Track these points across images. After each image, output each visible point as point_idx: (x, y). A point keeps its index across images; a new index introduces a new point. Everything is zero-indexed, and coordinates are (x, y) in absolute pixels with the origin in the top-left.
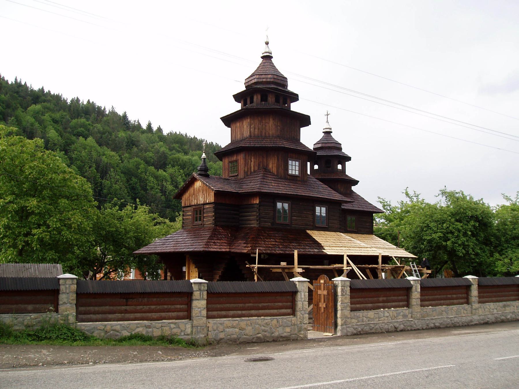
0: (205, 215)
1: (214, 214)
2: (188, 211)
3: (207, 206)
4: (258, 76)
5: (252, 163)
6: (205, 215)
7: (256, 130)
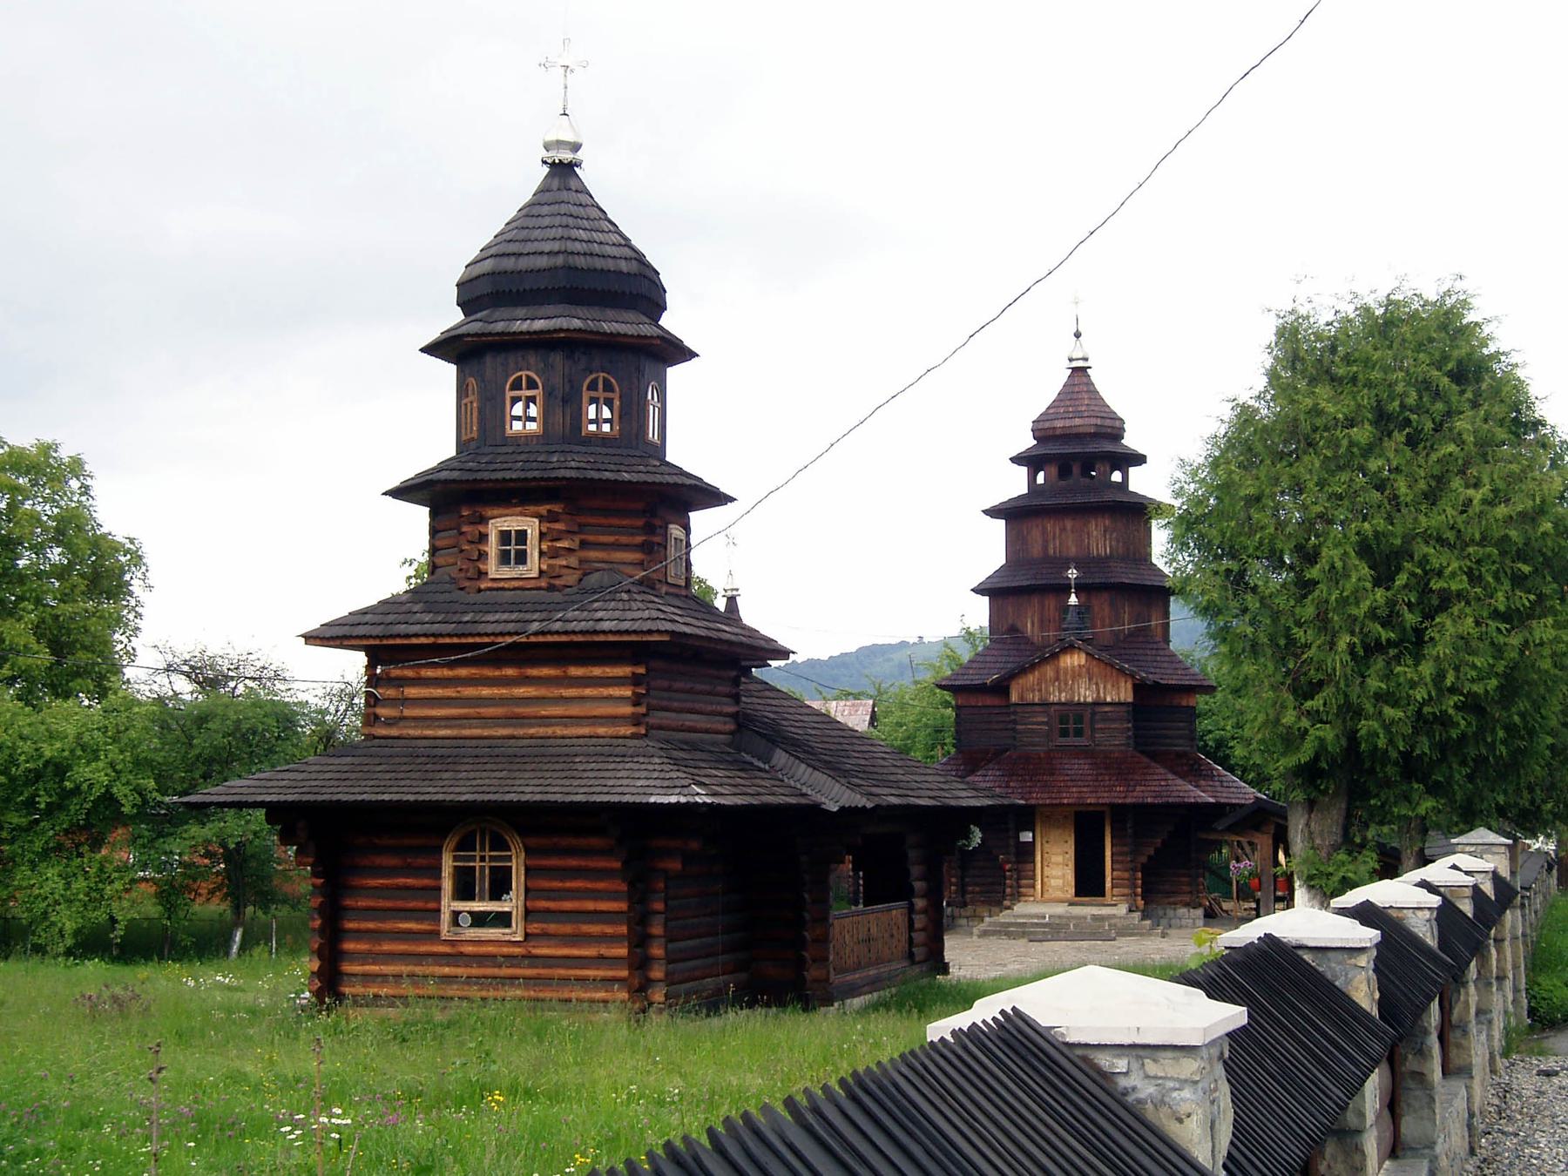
3: (1107, 709)
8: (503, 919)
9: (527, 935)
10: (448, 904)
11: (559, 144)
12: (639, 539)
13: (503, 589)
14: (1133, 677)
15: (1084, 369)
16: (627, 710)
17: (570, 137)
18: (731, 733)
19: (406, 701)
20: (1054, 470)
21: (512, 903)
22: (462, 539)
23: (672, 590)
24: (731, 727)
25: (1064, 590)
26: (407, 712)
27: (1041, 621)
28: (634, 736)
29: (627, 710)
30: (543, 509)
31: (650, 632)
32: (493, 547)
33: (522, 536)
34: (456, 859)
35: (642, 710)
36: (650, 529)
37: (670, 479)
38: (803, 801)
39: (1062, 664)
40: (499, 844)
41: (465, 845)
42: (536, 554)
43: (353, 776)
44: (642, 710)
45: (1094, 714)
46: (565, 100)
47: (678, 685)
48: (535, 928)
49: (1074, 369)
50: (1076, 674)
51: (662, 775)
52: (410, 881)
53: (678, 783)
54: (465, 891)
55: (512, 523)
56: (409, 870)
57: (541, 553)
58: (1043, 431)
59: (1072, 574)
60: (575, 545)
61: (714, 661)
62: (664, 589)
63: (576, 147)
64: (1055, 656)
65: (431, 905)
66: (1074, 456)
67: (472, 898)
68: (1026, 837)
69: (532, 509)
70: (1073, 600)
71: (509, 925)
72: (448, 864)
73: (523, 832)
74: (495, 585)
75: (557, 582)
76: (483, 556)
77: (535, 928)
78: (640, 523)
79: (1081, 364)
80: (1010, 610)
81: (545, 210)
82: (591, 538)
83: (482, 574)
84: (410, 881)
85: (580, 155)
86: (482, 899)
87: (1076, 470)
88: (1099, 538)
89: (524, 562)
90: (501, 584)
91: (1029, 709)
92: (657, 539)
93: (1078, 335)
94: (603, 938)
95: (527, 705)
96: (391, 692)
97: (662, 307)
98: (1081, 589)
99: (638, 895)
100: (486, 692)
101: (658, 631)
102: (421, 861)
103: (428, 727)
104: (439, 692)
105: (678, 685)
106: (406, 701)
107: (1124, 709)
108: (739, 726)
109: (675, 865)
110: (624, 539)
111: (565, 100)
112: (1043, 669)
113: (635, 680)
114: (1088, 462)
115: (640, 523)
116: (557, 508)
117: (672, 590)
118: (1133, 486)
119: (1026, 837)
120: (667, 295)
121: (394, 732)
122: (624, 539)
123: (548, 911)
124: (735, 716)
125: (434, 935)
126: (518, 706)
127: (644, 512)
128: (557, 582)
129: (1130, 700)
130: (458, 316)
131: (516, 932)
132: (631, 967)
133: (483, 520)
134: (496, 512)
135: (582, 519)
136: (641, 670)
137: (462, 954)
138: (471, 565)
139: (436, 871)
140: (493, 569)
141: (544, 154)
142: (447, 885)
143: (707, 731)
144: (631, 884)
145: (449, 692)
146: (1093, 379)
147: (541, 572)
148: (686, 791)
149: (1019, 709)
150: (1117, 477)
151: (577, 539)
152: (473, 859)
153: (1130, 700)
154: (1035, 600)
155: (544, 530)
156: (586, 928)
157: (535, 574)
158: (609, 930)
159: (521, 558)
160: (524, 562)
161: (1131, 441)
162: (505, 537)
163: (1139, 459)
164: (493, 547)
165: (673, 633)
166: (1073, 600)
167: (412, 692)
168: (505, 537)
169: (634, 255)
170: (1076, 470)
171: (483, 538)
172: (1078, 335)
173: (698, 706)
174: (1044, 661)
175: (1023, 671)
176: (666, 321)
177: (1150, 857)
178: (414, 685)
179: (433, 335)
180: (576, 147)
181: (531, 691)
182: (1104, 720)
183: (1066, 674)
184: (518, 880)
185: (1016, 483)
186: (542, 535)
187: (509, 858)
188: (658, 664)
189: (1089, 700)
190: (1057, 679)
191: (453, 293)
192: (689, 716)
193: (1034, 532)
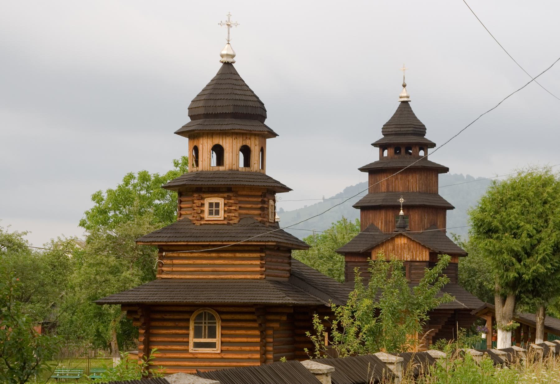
3: (417, 264)
8: (213, 345)
9: (222, 351)
10: (192, 340)
11: (228, 55)
12: (260, 206)
13: (210, 224)
14: (429, 249)
15: (406, 102)
16: (258, 269)
17: (231, 53)
18: (288, 277)
19: (173, 265)
20: (392, 151)
21: (217, 340)
22: (195, 205)
23: (271, 224)
24: (288, 275)
25: (397, 208)
26: (174, 269)
27: (386, 222)
28: (261, 279)
29: (258, 269)
30: (225, 195)
31: (268, 241)
32: (206, 208)
33: (217, 205)
34: (195, 323)
35: (264, 269)
36: (263, 202)
37: (273, 185)
38: (317, 303)
39: (396, 243)
40: (212, 317)
41: (199, 317)
42: (223, 212)
43: (159, 293)
44: (264, 269)
45: (411, 266)
46: (229, 37)
47: (273, 260)
48: (225, 348)
49: (403, 102)
50: (403, 248)
51: (274, 293)
52: (178, 331)
53: (281, 296)
54: (198, 334)
55: (214, 200)
56: (181, 328)
57: (225, 211)
58: (387, 130)
59: (402, 200)
60: (237, 208)
61: (280, 248)
62: (268, 224)
63: (233, 56)
64: (393, 239)
65: (185, 340)
66: (403, 144)
67: (201, 338)
69: (222, 195)
70: (401, 213)
71: (215, 347)
72: (192, 325)
73: (220, 313)
74: (207, 222)
75: (231, 222)
76: (202, 211)
77: (225, 348)
78: (260, 200)
79: (406, 99)
80: (371, 216)
81: (223, 82)
82: (242, 206)
83: (202, 218)
84: (178, 331)
85: (235, 59)
86: (205, 338)
87: (403, 151)
88: (414, 183)
89: (218, 214)
90: (210, 222)
92: (266, 206)
93: (404, 86)
94: (250, 352)
95: (220, 267)
96: (169, 262)
97: (264, 117)
98: (406, 207)
99: (263, 336)
100: (205, 262)
101: (272, 241)
102: (182, 324)
103: (182, 275)
104: (186, 262)
105: (273, 260)
106: (173, 265)
107: (425, 264)
108: (291, 275)
109: (276, 325)
110: (254, 206)
111: (229, 37)
112: (387, 245)
113: (261, 258)
114: (409, 146)
115: (260, 200)
116: (231, 194)
117: (271, 224)
118: (430, 158)
120: (267, 113)
121: (169, 276)
122: (254, 206)
123: (230, 342)
124: (289, 271)
125: (187, 351)
126: (216, 267)
127: (261, 196)
128: (231, 222)
129: (428, 259)
130: (189, 120)
131: (218, 349)
132: (261, 362)
133: (203, 199)
134: (207, 195)
135: (240, 199)
136: (263, 255)
137: (197, 358)
138: (198, 215)
139: (188, 328)
140: (206, 216)
141: (220, 58)
142: (192, 333)
143: (281, 277)
144: (261, 332)
145: (191, 262)
146: (411, 105)
147: (225, 218)
148: (284, 299)
150: (422, 153)
151: (238, 205)
152: (202, 323)
153: (428, 259)
154: (383, 213)
155: (226, 202)
156: (244, 348)
157: (222, 219)
158: (252, 348)
159: (217, 213)
160: (218, 214)
161: (429, 136)
162: (211, 205)
163: (433, 145)
164: (206, 208)
165: (277, 242)
166: (401, 213)
167: (175, 262)
168: (211, 205)
169: (256, 99)
170: (403, 151)
171: (203, 205)
172: (404, 86)
173: (279, 267)
174: (388, 241)
175: (378, 246)
176: (266, 122)
178: (177, 259)
179: (178, 127)
180: (233, 56)
181: (221, 262)
182: (416, 269)
183: (398, 247)
184: (218, 332)
185: (373, 156)
186: (225, 204)
187: (215, 323)
188: (268, 252)
189: (409, 259)
190: (394, 249)
191: (187, 111)
192: (277, 271)
193: (383, 180)
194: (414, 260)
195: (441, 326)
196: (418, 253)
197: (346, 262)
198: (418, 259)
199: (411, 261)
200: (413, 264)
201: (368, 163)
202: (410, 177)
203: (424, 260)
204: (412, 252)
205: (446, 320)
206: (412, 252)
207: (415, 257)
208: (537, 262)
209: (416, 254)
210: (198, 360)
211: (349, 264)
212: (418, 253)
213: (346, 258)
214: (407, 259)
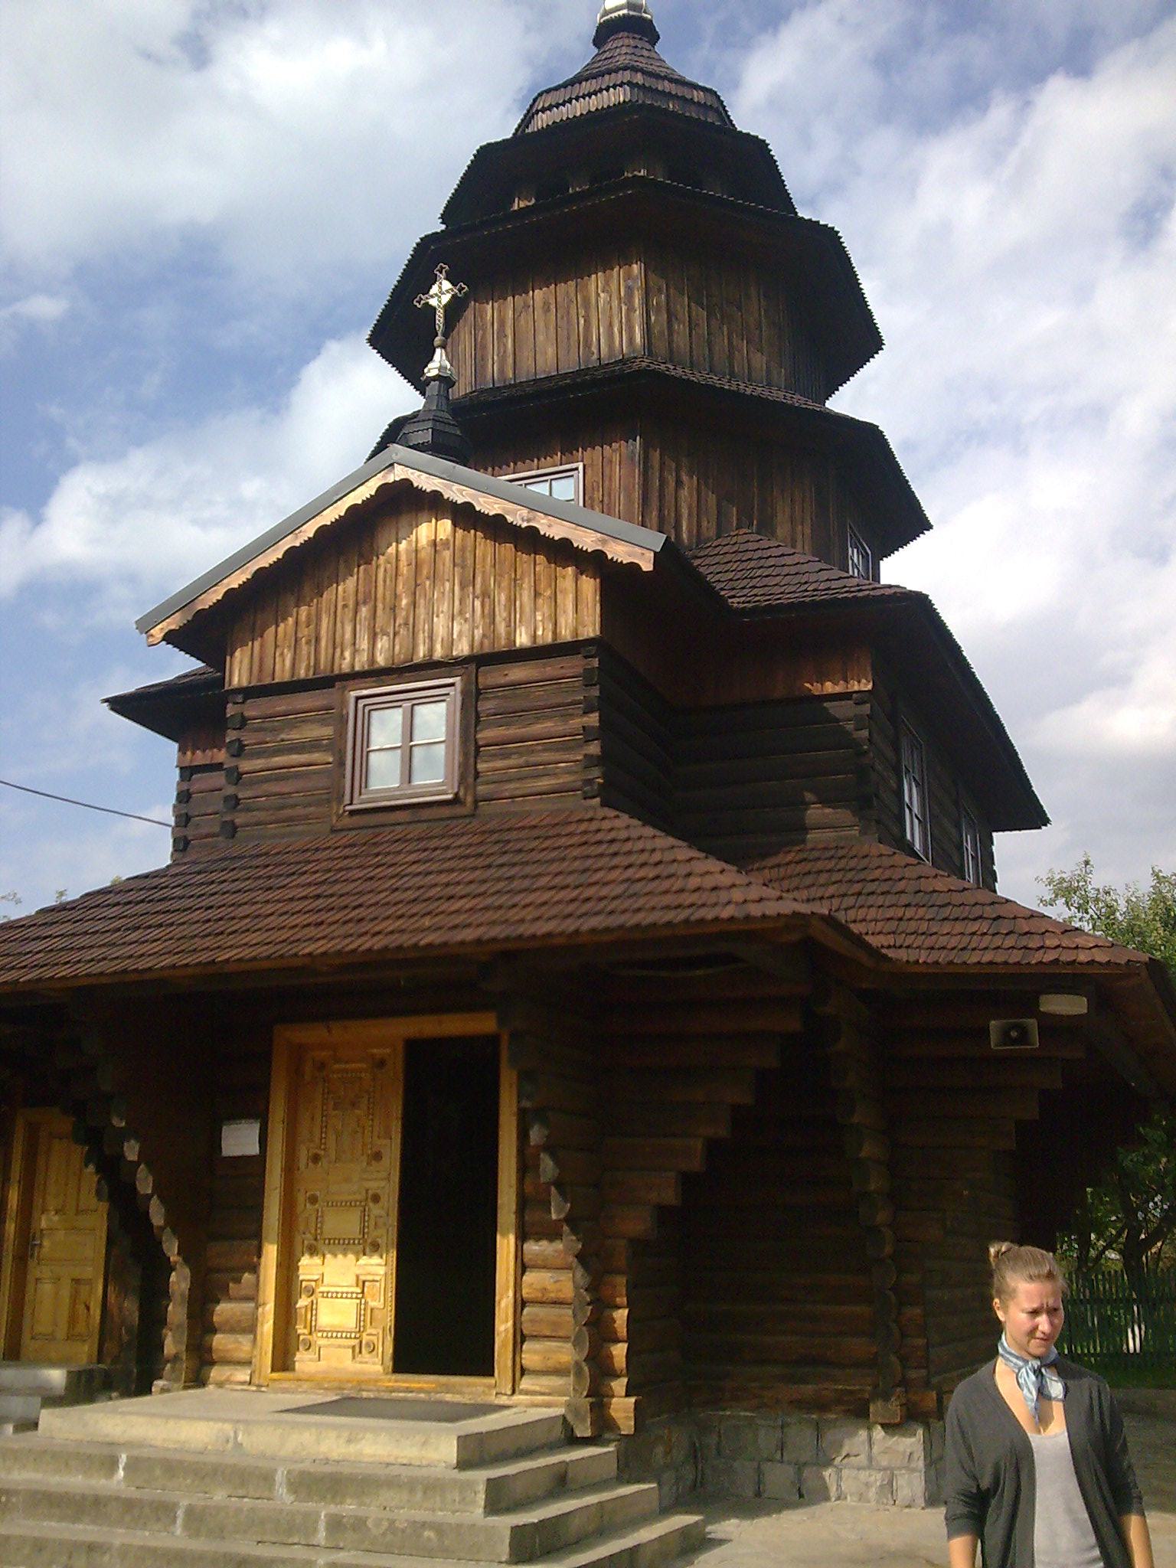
0: (486, 735)
1: (593, 719)
2: (298, 718)
3: (517, 673)
4: (639, 78)
5: (684, 493)
6: (486, 735)
7: (681, 328)
45: (472, 697)
50: (426, 571)
68: (240, 1140)
91: (281, 704)
107: (573, 665)
119: (240, 1140)
129: (591, 629)
149: (253, 709)
153: (591, 629)
177: (663, 1213)
182: (508, 716)
189: (462, 649)
194: (502, 645)
195: (699, 1145)
196: (526, 596)
197: (187, 772)
198: (522, 639)
199: (481, 660)
200: (492, 676)
201: (912, 545)
202: (595, 282)
203: (566, 634)
204: (485, 594)
205: (669, 1195)
206: (485, 594)
207: (501, 628)
208: (505, 1038)
209: (512, 601)
210: (130, 1308)
211: (202, 781)
212: (526, 596)
213: (182, 750)
214: (451, 643)
